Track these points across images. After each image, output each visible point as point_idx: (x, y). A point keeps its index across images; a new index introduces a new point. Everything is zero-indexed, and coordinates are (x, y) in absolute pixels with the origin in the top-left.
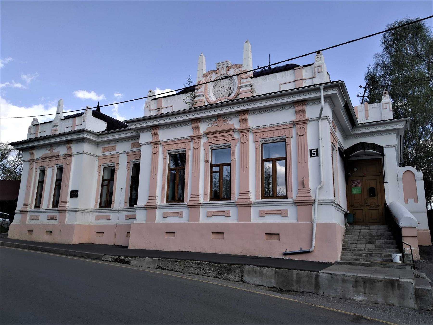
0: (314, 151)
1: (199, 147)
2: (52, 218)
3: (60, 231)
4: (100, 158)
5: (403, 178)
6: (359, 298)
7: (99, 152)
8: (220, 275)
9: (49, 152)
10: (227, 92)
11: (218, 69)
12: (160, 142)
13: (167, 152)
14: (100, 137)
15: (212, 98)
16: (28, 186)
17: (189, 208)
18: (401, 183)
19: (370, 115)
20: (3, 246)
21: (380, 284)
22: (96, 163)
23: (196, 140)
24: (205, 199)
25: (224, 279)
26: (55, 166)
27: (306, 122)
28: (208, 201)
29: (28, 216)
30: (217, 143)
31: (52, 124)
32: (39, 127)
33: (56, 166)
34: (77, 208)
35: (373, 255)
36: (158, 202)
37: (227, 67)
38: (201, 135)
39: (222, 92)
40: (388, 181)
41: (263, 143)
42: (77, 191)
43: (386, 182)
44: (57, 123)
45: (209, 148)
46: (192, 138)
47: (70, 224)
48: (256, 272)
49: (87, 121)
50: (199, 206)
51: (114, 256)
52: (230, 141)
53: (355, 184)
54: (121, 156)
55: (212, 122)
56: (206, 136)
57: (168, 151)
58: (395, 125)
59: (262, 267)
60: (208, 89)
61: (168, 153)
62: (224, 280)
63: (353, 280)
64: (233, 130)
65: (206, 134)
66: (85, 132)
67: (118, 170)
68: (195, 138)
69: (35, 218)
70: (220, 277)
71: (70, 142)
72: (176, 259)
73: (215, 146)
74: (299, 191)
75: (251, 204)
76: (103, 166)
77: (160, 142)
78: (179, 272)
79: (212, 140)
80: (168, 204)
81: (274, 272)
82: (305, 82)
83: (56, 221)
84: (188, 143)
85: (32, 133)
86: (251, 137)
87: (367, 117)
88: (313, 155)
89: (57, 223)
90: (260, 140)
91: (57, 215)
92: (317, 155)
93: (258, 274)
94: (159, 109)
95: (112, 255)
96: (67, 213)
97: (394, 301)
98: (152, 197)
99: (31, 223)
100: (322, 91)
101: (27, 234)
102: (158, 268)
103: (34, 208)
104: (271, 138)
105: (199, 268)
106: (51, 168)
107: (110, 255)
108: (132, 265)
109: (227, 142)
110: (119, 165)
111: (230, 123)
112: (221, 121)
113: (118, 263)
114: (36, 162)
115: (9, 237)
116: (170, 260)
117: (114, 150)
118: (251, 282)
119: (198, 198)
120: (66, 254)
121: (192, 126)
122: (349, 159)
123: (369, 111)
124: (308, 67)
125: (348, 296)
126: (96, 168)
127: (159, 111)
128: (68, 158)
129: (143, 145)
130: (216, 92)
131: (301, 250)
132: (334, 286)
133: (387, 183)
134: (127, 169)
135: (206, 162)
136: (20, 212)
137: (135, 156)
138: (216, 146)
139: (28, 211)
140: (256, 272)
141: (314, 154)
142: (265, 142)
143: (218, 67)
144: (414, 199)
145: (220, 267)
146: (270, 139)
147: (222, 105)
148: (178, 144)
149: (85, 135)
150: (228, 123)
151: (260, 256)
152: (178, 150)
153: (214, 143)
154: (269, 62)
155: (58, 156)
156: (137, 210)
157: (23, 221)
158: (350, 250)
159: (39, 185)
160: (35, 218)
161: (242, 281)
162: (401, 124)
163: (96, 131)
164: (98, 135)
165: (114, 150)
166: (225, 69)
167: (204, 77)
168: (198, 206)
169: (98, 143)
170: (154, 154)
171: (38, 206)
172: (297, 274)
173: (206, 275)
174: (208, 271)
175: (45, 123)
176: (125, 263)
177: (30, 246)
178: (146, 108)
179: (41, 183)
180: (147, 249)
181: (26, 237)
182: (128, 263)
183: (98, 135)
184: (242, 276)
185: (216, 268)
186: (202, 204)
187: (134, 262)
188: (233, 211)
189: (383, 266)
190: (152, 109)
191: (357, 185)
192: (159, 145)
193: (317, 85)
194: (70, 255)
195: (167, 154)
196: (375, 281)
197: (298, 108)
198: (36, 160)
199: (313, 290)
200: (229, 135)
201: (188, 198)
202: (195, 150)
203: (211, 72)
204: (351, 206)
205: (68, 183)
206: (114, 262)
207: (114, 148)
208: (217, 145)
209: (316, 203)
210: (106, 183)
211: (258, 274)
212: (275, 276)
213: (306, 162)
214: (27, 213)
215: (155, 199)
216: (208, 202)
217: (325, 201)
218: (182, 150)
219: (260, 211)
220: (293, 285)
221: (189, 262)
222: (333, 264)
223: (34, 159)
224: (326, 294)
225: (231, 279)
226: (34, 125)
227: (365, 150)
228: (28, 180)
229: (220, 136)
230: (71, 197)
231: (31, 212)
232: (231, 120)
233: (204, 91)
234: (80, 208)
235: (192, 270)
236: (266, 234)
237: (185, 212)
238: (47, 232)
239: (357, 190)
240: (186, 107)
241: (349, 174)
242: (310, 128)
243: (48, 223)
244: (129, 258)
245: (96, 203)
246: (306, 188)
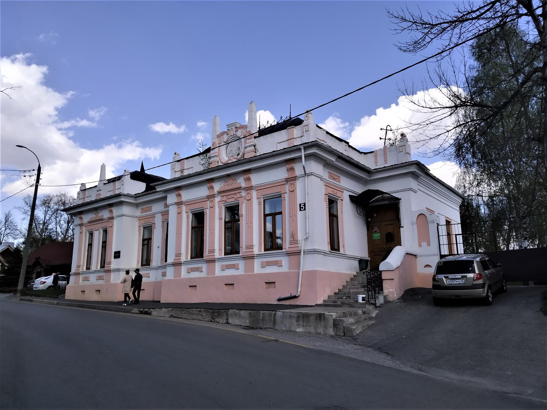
0: (302, 205)
1: (214, 206)
2: (100, 278)
3: (107, 290)
4: (140, 218)
5: (417, 222)
6: (300, 330)
7: (138, 212)
8: (214, 319)
9: (95, 216)
10: (237, 151)
11: (229, 130)
12: (253, 187)
13: (189, 211)
14: (138, 198)
15: (225, 158)
16: (80, 249)
17: (207, 263)
18: (415, 226)
19: (388, 159)
20: (58, 305)
21: (312, 318)
22: (137, 224)
23: (292, 182)
24: (220, 254)
25: (216, 322)
26: (101, 229)
27: (295, 178)
28: (222, 256)
29: (81, 277)
30: (228, 201)
31: (97, 189)
32: (86, 192)
33: (102, 229)
34: (120, 268)
35: (351, 297)
36: (183, 259)
37: (236, 128)
38: (215, 195)
39: (233, 152)
40: (440, 222)
41: (265, 199)
42: (119, 252)
43: (402, 226)
44: (100, 187)
45: (223, 206)
46: (287, 180)
47: (114, 283)
48: (236, 315)
49: (125, 184)
50: (215, 261)
51: (140, 308)
52: (239, 199)
53: (375, 230)
54: (157, 215)
55: (224, 182)
56: (219, 195)
57: (190, 211)
58: (407, 169)
59: (241, 310)
60: (221, 150)
61: (263, 198)
62: (216, 323)
63: (296, 315)
64: (239, 188)
65: (220, 192)
66: (122, 196)
67: (155, 230)
68: (211, 197)
69: (86, 279)
70: (213, 320)
71: (111, 205)
72: (184, 308)
73: (227, 204)
74: (291, 243)
75: (215, 260)
76: (143, 226)
77: (253, 187)
78: (186, 319)
79: (225, 198)
80: (191, 260)
81: (248, 313)
82: (296, 140)
83: (104, 280)
84: (284, 186)
85: (81, 198)
86: (254, 194)
87: (386, 161)
88: (301, 209)
89: (104, 283)
90: (262, 197)
91: (103, 276)
92: (305, 209)
93: (238, 316)
94: (182, 171)
95: (138, 308)
96: (112, 273)
97: (321, 330)
98: (178, 255)
99: (83, 284)
100: (303, 150)
101: (81, 295)
102: (171, 317)
103: (141, 266)
104: (271, 195)
105: (200, 314)
106: (98, 231)
107: (137, 308)
108: (153, 316)
109: (236, 199)
110: (156, 225)
111: (238, 181)
112: (231, 180)
113: (143, 315)
114: (85, 225)
115: (66, 298)
116: (179, 309)
117: (151, 211)
118: (233, 323)
119: (213, 253)
120: (105, 309)
121: (207, 186)
122: (369, 205)
123: (378, 157)
124: (275, 133)
125: (293, 329)
126: (137, 228)
127: (182, 172)
128: (110, 221)
129: (171, 205)
130: (228, 152)
131: (291, 295)
132: (284, 322)
133: (403, 227)
134: (162, 229)
135: (220, 219)
136: (74, 274)
137: (144, 220)
138: (228, 203)
139: (80, 272)
140: (236, 315)
141: (302, 208)
142: (267, 198)
143: (229, 129)
144: (427, 243)
145: (213, 313)
146: (269, 195)
147: (228, 166)
148: (278, 186)
149: (123, 199)
150: (237, 182)
151: (261, 303)
152: (198, 209)
153: (226, 201)
154: (290, 112)
155: (102, 219)
156: (167, 267)
157: (77, 282)
158: (341, 294)
159: (89, 248)
160: (86, 279)
161: (227, 323)
162: (412, 167)
163: (133, 193)
164: (135, 197)
165: (151, 211)
166: (234, 129)
167: (217, 138)
168: (252, 257)
169: (137, 204)
170: (211, 207)
171: (88, 268)
172: (263, 314)
173: (204, 320)
174: (205, 317)
175: (90, 188)
176: (148, 315)
177: (79, 304)
178: (172, 170)
179: (90, 245)
180: (175, 302)
181: (79, 297)
182: (150, 314)
183: (135, 197)
184: (228, 319)
185: (211, 313)
186: (217, 258)
187: (155, 313)
188: (285, 260)
189: (349, 306)
190: (177, 171)
191: (376, 231)
192: (183, 205)
193: (310, 142)
194: (109, 310)
195: (190, 213)
196: (310, 315)
197: (288, 166)
198: (85, 224)
199: (272, 327)
200: (237, 193)
201: (243, 250)
202: (210, 208)
203: (223, 133)
204: (372, 252)
205: (112, 244)
206: (140, 313)
207: (150, 209)
208: (229, 203)
209: (302, 253)
210: (146, 242)
211: (238, 316)
212: (249, 317)
213: (296, 216)
214: (80, 275)
215: (180, 256)
216: (263, 252)
217: (309, 251)
218: (277, 194)
219: (262, 262)
220: (260, 323)
221: (193, 310)
222: (314, 307)
223: (83, 224)
224: (279, 329)
225: (221, 322)
226: (82, 190)
227: (383, 195)
228: (177, 226)
229: (231, 194)
230: (115, 257)
231: (83, 273)
232: (238, 179)
233: (218, 152)
234: (122, 267)
235: (194, 316)
236: (266, 283)
237: (241, 264)
238: (97, 291)
239: (377, 236)
240: (201, 169)
241: (369, 220)
242: (299, 184)
243: (97, 283)
244: (151, 310)
245: (138, 262)
246: (295, 240)
